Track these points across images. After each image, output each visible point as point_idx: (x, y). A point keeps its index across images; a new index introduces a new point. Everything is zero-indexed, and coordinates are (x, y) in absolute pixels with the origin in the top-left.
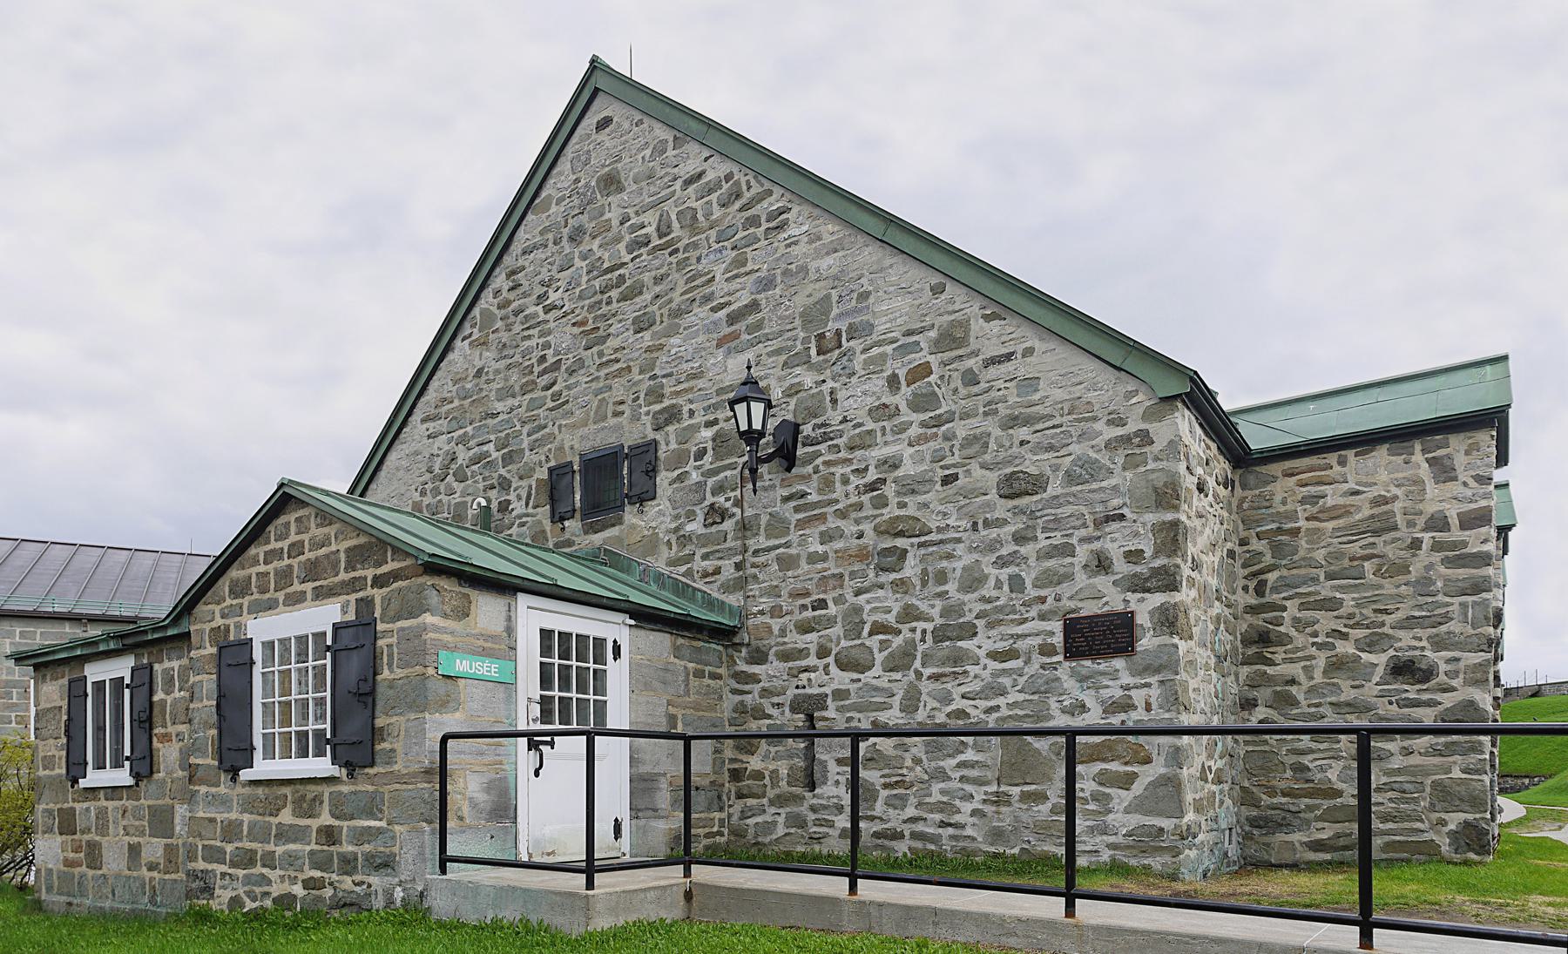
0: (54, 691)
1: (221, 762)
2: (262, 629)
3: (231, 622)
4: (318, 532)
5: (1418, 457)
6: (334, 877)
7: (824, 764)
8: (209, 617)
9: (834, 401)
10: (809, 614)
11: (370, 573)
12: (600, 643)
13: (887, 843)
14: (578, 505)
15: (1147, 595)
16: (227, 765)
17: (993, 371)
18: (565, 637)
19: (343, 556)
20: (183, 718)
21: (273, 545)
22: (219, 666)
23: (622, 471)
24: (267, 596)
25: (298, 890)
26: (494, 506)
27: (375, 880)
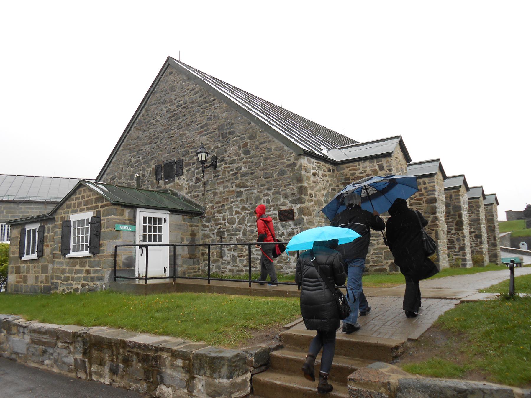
0: (16, 232)
1: (61, 253)
2: (74, 217)
3: (66, 215)
4: (88, 193)
5: (376, 164)
6: (89, 283)
7: (225, 251)
8: (60, 214)
9: (226, 151)
10: (220, 208)
11: (100, 204)
12: (160, 219)
13: (240, 273)
14: (163, 176)
15: (296, 205)
16: (63, 253)
17: (261, 146)
18: (150, 218)
19: (94, 200)
20: (52, 240)
21: (77, 196)
22: (62, 227)
24: (75, 209)
25: (80, 287)
26: (141, 176)
27: (98, 283)
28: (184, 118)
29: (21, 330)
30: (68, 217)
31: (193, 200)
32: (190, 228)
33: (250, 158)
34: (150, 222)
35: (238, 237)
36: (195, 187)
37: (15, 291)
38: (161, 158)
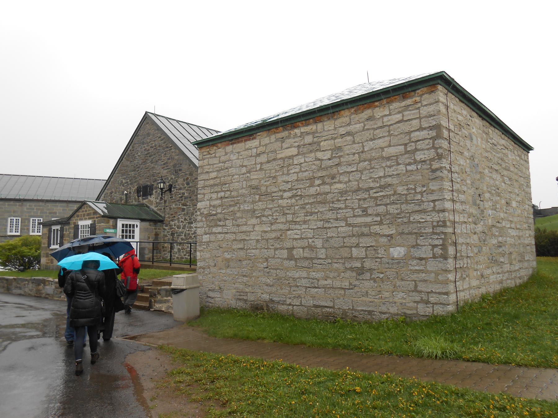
2: (81, 223)
8: (73, 220)
11: (95, 216)
12: (134, 225)
18: (127, 225)
21: (83, 210)
23: (103, 223)
28: (155, 156)
29: (50, 283)
30: (78, 222)
31: (158, 212)
32: (154, 231)
33: (190, 187)
34: (126, 227)
35: (182, 237)
36: (160, 203)
37: (46, 269)
38: (141, 182)
